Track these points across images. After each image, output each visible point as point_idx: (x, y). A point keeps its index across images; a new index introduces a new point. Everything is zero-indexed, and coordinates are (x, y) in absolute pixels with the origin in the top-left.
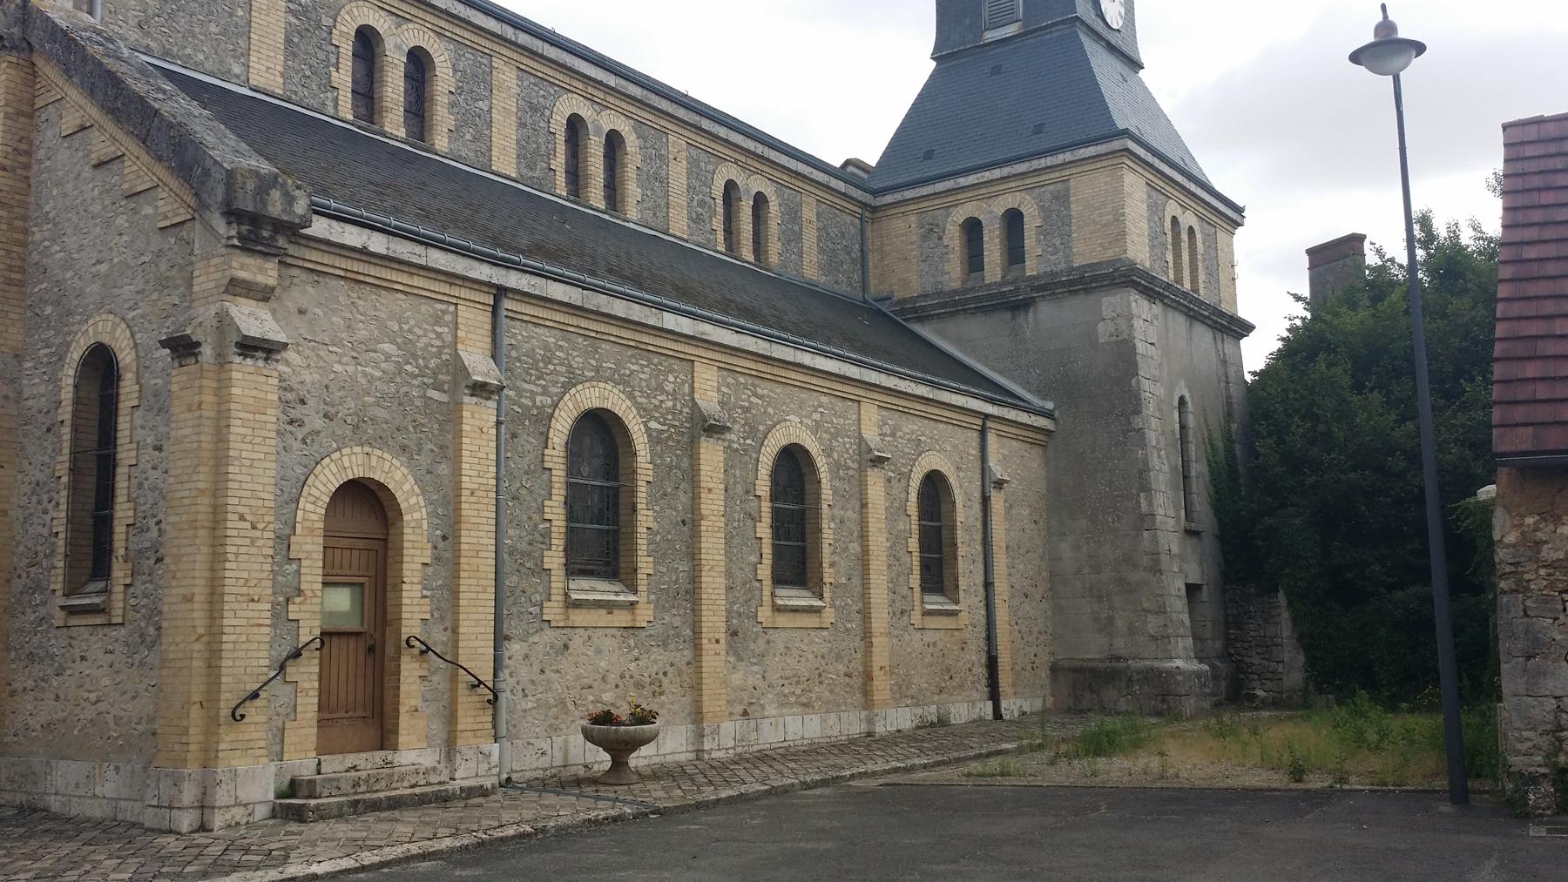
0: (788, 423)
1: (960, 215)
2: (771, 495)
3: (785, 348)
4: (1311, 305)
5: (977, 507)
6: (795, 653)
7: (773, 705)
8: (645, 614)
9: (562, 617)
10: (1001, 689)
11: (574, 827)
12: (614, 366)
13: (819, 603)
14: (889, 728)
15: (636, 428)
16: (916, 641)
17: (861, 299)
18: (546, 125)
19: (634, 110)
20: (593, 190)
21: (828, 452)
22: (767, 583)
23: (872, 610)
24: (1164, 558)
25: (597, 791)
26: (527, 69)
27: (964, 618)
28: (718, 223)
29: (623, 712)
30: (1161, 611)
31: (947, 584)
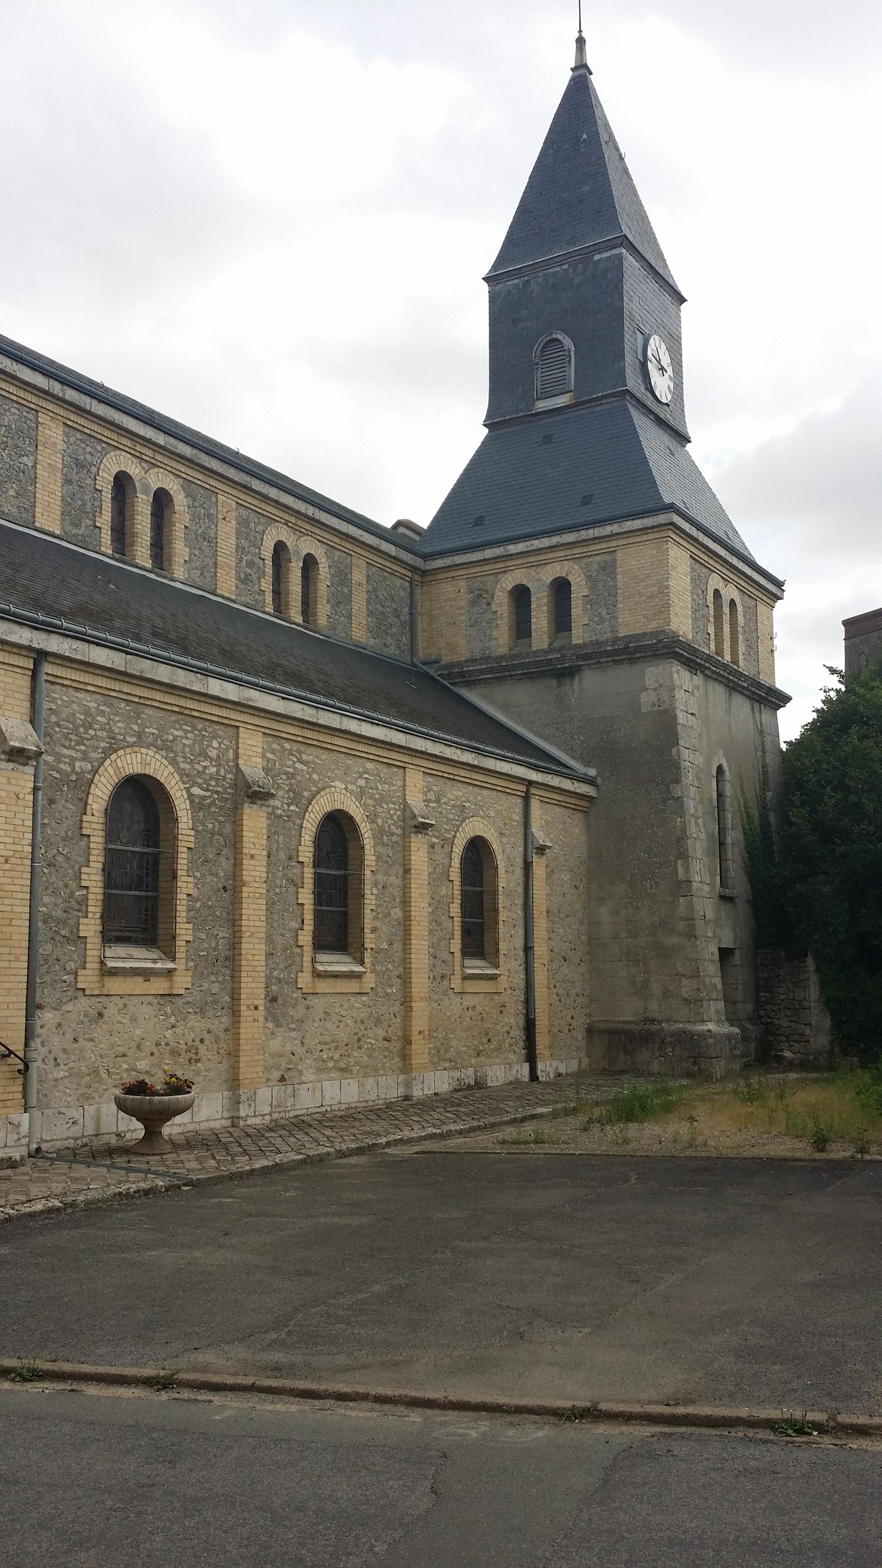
0: (333, 789)
1: (509, 581)
2: (314, 861)
3: (331, 715)
4: (845, 678)
5: (519, 872)
6: (335, 1018)
7: (311, 1071)
8: (182, 982)
9: (98, 985)
10: (537, 1052)
11: (103, 1201)
12: (156, 732)
13: (360, 969)
14: (426, 1092)
15: (178, 794)
16: (455, 1005)
17: (409, 662)
18: (92, 482)
19: (183, 469)
20: (139, 548)
21: (372, 818)
22: (308, 949)
23: (413, 975)
24: (699, 923)
25: (129, 1162)
26: (74, 425)
27: (503, 982)
28: (267, 585)
29: (157, 1081)
30: (695, 975)
31: (488, 948)
